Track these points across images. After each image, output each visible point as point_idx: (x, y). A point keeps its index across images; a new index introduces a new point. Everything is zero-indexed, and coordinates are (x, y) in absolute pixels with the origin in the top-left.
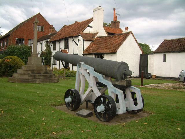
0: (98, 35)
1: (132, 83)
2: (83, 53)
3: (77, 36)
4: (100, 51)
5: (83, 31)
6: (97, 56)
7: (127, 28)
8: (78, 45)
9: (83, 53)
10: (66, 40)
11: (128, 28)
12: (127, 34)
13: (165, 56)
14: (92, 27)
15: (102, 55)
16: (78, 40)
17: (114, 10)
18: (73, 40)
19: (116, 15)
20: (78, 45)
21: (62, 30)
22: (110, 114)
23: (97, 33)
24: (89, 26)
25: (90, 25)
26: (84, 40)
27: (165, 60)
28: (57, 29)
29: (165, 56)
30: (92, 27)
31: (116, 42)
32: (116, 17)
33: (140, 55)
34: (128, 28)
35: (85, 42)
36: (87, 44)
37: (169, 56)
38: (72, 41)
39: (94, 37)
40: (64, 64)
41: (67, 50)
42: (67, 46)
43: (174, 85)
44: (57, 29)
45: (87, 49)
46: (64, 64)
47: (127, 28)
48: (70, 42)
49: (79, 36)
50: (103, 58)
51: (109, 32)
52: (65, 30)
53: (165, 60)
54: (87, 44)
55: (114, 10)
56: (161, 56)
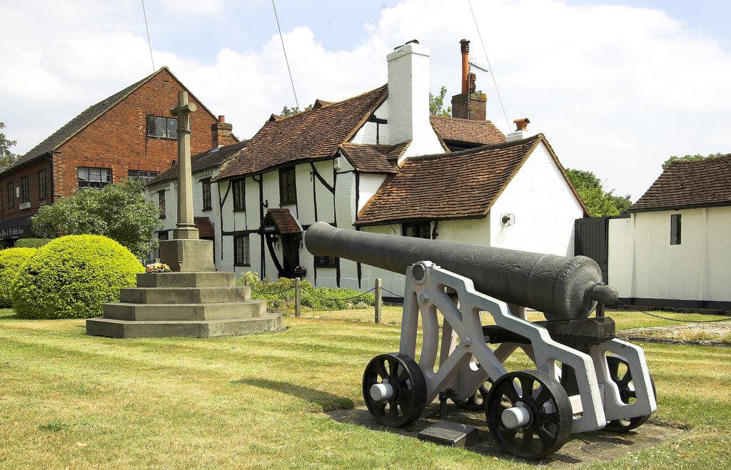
0: (412, 151)
1: (618, 331)
2: (357, 218)
3: (332, 158)
4: (417, 212)
5: (353, 137)
6: (410, 230)
7: (522, 124)
8: (333, 190)
9: (354, 220)
10: (286, 171)
11: (527, 121)
12: (524, 147)
13: (378, 142)
14: (384, 122)
15: (432, 227)
16: (335, 173)
17: (465, 45)
18: (315, 173)
19: (473, 71)
20: (333, 190)
21: (261, 135)
22: (550, 430)
23: (404, 145)
24: (372, 119)
25: (379, 114)
26: (357, 174)
27: (677, 237)
28: (245, 128)
29: (378, 142)
30: (384, 122)
31: (482, 178)
32: (473, 77)
33: (577, 222)
34: (527, 121)
35: (363, 181)
36: (369, 190)
37: (692, 222)
38: (309, 176)
39: (396, 160)
40: (281, 263)
41: (292, 210)
42: (289, 195)
43: (701, 331)
44: (245, 128)
45: (373, 204)
46: (281, 263)
47: (522, 124)
48: (303, 181)
49: (339, 155)
50: (435, 235)
51: (449, 137)
52: (276, 134)
53: (677, 237)
54: (369, 190)
55: (465, 45)
56: (660, 223)
